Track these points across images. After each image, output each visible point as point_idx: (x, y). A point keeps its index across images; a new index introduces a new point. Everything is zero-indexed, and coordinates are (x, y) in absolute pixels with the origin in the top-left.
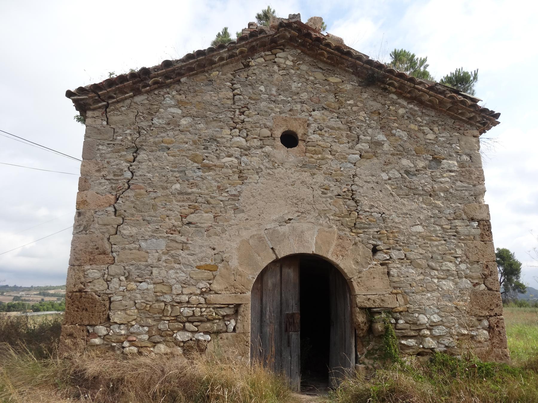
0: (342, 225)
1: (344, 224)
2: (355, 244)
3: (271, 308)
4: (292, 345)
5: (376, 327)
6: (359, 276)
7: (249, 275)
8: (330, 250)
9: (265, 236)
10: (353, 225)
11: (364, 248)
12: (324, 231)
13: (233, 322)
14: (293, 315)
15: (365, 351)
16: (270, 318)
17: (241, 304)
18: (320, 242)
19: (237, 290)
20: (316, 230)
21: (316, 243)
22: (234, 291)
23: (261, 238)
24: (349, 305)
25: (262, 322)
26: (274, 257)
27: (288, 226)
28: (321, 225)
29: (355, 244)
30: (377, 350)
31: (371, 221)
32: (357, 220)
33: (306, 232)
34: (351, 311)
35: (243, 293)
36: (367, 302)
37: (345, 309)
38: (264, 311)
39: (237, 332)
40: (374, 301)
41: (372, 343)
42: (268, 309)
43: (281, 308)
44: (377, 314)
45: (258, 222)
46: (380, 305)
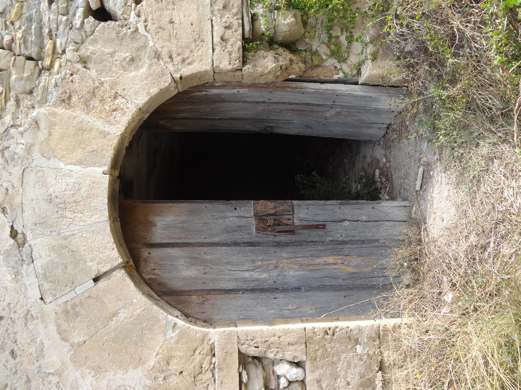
0: (31, 92)
1: (28, 88)
2: (85, 62)
3: (245, 268)
4: (321, 218)
5: (285, 29)
6: (167, 59)
7: (168, 337)
8: (101, 127)
9: (61, 301)
10: (31, 64)
11: (95, 41)
12: (47, 140)
13: (282, 369)
14: (260, 218)
15: (332, 62)
16: (264, 271)
17: (239, 352)
18: (78, 154)
19: (206, 366)
20: (44, 162)
21: (80, 163)
22: (209, 375)
23: (66, 312)
24: (235, 91)
25: (277, 289)
26: (121, 274)
27: (34, 238)
28: (29, 149)
29: (84, 61)
30: (330, 37)
31: (19, 16)
32: (17, 53)
33: (51, 191)
34: (249, 86)
35: (212, 349)
36: (230, 43)
37: (245, 102)
38: (252, 285)
39: (304, 358)
40: (227, 28)
41: (315, 45)
42: (247, 275)
43: (244, 243)
44: (257, 24)
45: (20, 323)
46: (236, 14)
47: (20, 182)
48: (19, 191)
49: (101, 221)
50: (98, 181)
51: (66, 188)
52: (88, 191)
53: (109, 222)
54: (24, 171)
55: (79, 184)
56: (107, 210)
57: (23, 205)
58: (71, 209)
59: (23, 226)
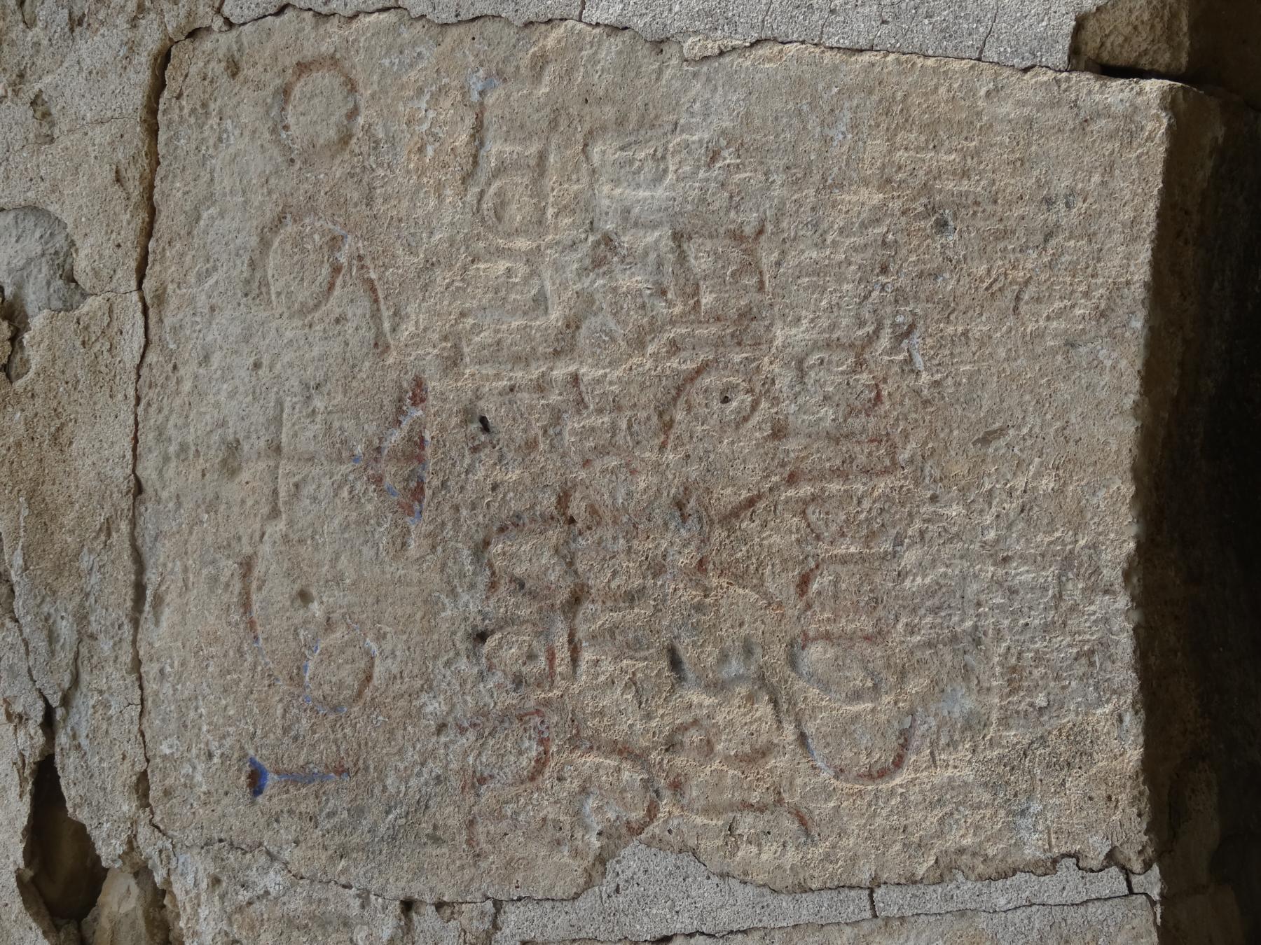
47: (129, 224)
48: (111, 332)
49: (1034, 845)
50: (1009, 183)
51: (587, 300)
52: (860, 352)
53: (1152, 883)
54: (158, 85)
55: (737, 236)
56: (1124, 675)
57: (148, 511)
58: (641, 611)
59: (141, 786)
